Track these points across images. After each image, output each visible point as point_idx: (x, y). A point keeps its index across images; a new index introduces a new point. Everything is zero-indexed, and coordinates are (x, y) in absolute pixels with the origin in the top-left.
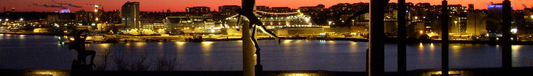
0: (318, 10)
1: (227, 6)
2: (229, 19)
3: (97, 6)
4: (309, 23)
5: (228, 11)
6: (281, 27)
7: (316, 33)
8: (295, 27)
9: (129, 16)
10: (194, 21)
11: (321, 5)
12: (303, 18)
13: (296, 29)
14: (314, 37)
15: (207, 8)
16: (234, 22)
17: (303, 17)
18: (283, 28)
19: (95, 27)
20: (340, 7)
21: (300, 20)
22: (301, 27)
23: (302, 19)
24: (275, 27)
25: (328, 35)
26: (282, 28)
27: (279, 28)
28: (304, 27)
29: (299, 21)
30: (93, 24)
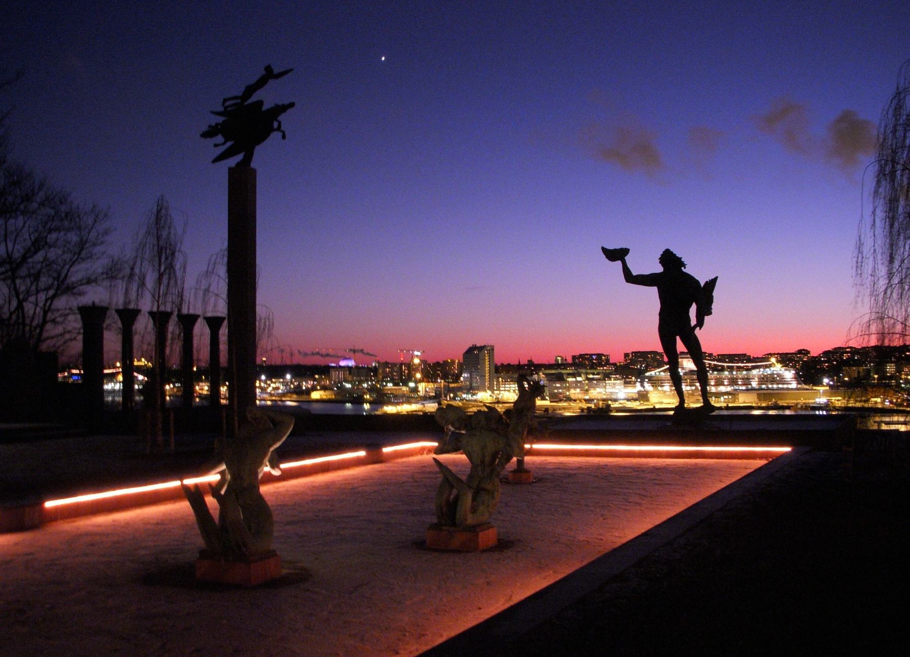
0: (798, 359)
1: (639, 352)
2: (651, 374)
3: (419, 354)
4: (791, 381)
5: (640, 361)
6: (744, 388)
7: (805, 400)
8: (768, 389)
9: (476, 369)
10: (588, 379)
11: (804, 350)
12: (781, 372)
13: (769, 391)
14: (806, 406)
15: (604, 356)
16: (661, 380)
17: (781, 370)
18: (747, 390)
19: (416, 390)
20: (837, 353)
21: (775, 376)
22: (778, 389)
23: (779, 375)
24: (732, 388)
25: (831, 402)
26: (744, 390)
27: (739, 390)
28: (783, 389)
29: (774, 378)
30: (412, 385)
